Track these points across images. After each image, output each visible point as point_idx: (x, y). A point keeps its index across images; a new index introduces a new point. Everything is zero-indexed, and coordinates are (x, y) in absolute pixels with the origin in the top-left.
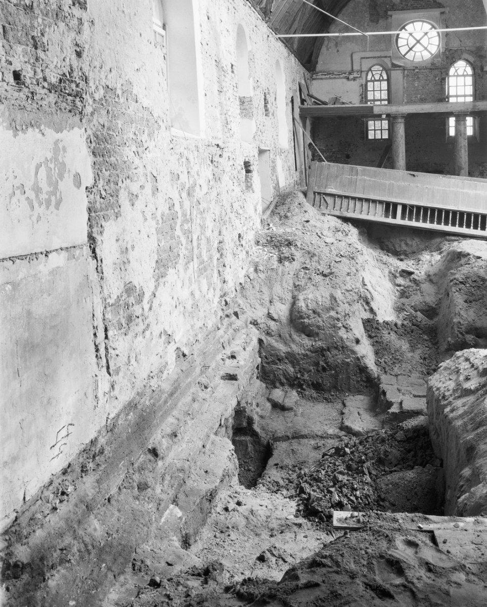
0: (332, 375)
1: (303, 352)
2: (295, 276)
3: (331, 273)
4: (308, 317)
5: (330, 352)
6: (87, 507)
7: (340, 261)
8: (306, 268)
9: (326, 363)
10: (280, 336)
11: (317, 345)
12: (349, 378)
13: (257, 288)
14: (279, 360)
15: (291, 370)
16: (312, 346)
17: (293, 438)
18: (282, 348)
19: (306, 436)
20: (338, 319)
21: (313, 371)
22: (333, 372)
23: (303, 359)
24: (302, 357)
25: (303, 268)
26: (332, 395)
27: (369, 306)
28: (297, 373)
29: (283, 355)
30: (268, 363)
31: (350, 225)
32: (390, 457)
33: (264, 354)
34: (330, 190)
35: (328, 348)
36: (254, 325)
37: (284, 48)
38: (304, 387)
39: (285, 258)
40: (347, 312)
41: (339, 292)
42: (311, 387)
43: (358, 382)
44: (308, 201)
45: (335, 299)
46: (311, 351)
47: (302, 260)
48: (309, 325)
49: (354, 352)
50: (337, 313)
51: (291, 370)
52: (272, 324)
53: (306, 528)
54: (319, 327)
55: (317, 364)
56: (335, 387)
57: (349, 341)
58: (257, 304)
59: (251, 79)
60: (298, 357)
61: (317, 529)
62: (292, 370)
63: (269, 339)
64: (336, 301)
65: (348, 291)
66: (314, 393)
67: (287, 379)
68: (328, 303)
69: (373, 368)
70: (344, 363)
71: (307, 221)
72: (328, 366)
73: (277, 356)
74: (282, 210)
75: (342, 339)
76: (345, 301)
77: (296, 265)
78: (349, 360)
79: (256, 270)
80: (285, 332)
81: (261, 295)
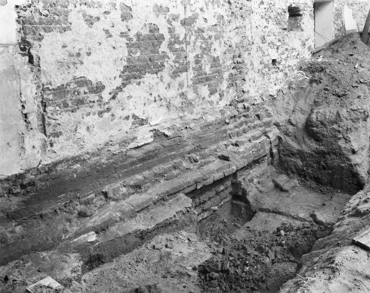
0: (329, 174)
1: (310, 152)
2: (317, 95)
3: (344, 95)
4: (317, 126)
5: (330, 156)
6: (7, 215)
7: (357, 87)
8: (327, 90)
9: (326, 164)
10: (296, 137)
11: (320, 149)
12: (342, 179)
13: (286, 100)
14: (292, 154)
15: (300, 163)
16: (317, 148)
17: (273, 212)
18: (295, 146)
19: (282, 213)
20: (339, 132)
21: (315, 167)
22: (330, 171)
23: (309, 157)
24: (309, 155)
25: (324, 89)
26: (327, 189)
28: (304, 166)
29: (296, 151)
30: (284, 155)
32: (299, 248)
33: (282, 148)
35: (328, 152)
36: (277, 126)
38: (307, 178)
39: (315, 80)
40: (349, 127)
41: (344, 110)
42: (313, 179)
43: (349, 183)
44: (362, 40)
45: (339, 115)
46: (315, 152)
47: (327, 83)
48: (317, 132)
49: (349, 160)
50: (339, 126)
51: (300, 163)
52: (290, 128)
53: (191, 280)
54: (323, 135)
55: (319, 163)
56: (331, 184)
57: (346, 150)
58: (282, 111)
60: (305, 154)
61: (198, 285)
62: (301, 163)
63: (287, 138)
64: (340, 117)
66: (314, 185)
67: (297, 169)
68: (333, 118)
69: (364, 175)
70: (339, 166)
71: (352, 55)
72: (327, 166)
73: (291, 151)
74: (335, 47)
75: (340, 147)
76: (349, 118)
77: (321, 86)
78: (344, 165)
79: (289, 88)
80: (300, 135)
81: (287, 106)
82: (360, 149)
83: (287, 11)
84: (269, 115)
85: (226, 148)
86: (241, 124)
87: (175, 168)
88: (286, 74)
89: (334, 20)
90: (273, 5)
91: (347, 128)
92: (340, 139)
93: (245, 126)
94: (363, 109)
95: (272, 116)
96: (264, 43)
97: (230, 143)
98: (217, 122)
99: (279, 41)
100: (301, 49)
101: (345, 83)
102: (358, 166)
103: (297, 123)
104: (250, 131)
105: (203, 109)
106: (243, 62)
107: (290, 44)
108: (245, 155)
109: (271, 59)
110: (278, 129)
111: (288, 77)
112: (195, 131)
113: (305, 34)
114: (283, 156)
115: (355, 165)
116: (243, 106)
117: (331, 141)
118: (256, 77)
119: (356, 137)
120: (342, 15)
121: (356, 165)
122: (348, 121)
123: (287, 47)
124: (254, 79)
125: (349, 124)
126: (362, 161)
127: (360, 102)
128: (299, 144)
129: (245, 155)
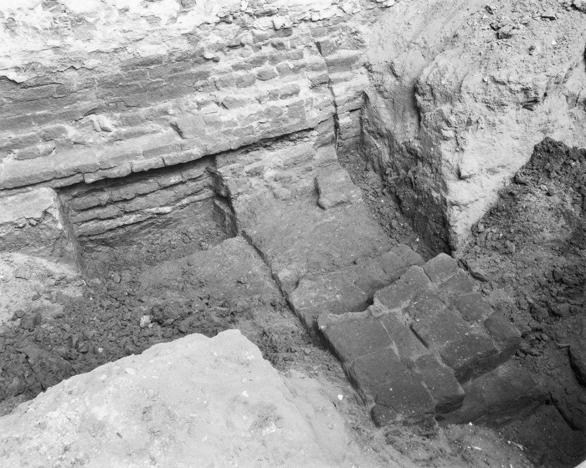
20: (448, 123)
29: (385, 132)
30: (369, 132)
33: (367, 117)
40: (474, 119)
43: (435, 234)
49: (446, 189)
52: (390, 79)
63: (380, 99)
76: (480, 97)
82: (484, 170)
84: (359, 44)
85: (199, 109)
86: (259, 62)
87: (46, 139)
92: (446, 139)
93: (267, 66)
94: (519, 84)
95: (364, 47)
97: (213, 98)
98: (174, 58)
102: (457, 208)
103: (403, 74)
104: (277, 78)
105: (124, 31)
108: (235, 128)
110: (370, 76)
112: (104, 75)
114: (367, 134)
115: (453, 204)
116: (271, 23)
117: (430, 137)
119: (483, 145)
121: (454, 205)
122: (477, 105)
125: (478, 110)
126: (473, 200)
127: (524, 65)
128: (395, 120)
129: (235, 128)
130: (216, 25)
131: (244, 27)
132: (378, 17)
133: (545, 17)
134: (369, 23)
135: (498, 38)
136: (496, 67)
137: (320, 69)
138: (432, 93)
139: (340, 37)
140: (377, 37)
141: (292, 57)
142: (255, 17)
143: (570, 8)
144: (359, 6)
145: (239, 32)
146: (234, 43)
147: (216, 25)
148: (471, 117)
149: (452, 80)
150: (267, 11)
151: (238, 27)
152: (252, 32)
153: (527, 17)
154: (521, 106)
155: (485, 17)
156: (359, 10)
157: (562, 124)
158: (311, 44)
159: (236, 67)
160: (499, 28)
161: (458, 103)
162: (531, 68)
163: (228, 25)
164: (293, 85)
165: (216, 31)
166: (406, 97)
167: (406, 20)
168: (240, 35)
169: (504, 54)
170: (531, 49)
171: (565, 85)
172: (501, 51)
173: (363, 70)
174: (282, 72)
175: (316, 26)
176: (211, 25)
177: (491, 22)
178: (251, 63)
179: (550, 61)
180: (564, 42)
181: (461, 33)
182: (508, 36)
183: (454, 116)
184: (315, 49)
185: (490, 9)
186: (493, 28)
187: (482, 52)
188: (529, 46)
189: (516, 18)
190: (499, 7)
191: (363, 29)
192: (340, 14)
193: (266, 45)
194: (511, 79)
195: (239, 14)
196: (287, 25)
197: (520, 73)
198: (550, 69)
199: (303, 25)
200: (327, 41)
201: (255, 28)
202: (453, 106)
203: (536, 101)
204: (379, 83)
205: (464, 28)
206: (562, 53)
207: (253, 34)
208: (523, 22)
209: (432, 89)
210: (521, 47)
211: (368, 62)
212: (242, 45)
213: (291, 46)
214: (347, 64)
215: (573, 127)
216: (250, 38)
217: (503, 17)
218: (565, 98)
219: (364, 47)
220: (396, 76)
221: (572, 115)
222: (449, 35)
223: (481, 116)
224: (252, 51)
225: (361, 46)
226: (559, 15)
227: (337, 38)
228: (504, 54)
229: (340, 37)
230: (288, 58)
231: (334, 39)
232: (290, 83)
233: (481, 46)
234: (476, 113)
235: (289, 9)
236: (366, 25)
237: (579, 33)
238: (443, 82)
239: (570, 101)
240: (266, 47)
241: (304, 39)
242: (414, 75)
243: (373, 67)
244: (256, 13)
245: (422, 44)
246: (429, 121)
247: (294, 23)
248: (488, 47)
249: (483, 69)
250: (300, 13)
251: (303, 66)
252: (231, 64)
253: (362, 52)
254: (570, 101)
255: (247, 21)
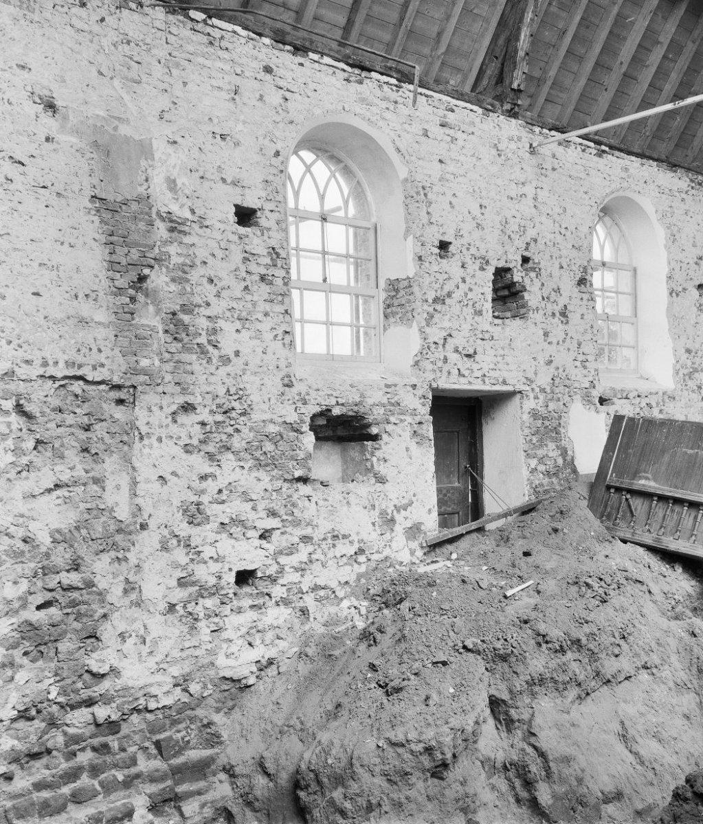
27: (529, 791)
31: (679, 570)
34: (642, 482)
37: (670, 174)
52: (261, 781)
59: (411, 238)
63: (249, 814)
65: (394, 744)
76: (377, 769)
83: (306, 428)
84: (214, 740)
86: (72, 775)
88: (304, 612)
89: (526, 447)
90: (244, 414)
91: (369, 801)
93: (85, 780)
95: (221, 743)
96: (199, 524)
99: (273, 514)
100: (374, 535)
101: (420, 648)
104: (101, 796)
106: (90, 584)
107: (321, 522)
109: (230, 570)
110: (232, 783)
111: (311, 619)
113: (393, 493)
118: (151, 627)
120: (562, 430)
123: (308, 531)
124: (142, 632)
127: (421, 718)
130: (12, 723)
131: (52, 723)
132: (237, 701)
133: (437, 663)
134: (226, 710)
135: (388, 696)
136: (390, 726)
137: (162, 779)
138: (318, 781)
139: (187, 732)
140: (238, 727)
141: (121, 765)
142: (68, 709)
143: (461, 650)
144: (210, 686)
145: (45, 732)
146: (36, 750)
147: (12, 723)
148: (371, 798)
149: (341, 755)
150: (85, 698)
151: (43, 725)
152: (63, 731)
153: (417, 665)
154: (429, 775)
155: (369, 675)
156: (211, 691)
157: (485, 800)
158: (147, 744)
159: (39, 786)
160: (387, 685)
161: (351, 783)
162: (430, 720)
163: (29, 723)
164: (124, 804)
165: (11, 732)
166: (286, 803)
167: (274, 699)
168: (46, 737)
169: (396, 709)
170: (427, 698)
171: (476, 746)
172: (394, 707)
173: (223, 776)
174: (108, 788)
175: (154, 718)
176: (4, 723)
177: (377, 680)
178: (61, 777)
179: (449, 709)
180: (462, 688)
181: (345, 701)
182: (398, 690)
183: (349, 801)
184: (154, 751)
185: (374, 666)
186: (380, 686)
187: (371, 713)
188: (424, 697)
189: (404, 670)
190: (384, 662)
191: (218, 718)
192: (185, 698)
193: (83, 750)
194: (410, 737)
195: (45, 705)
196: (114, 717)
197: (419, 729)
198: (451, 719)
199: (135, 718)
200: (171, 738)
201: (67, 725)
202: (346, 788)
203: (445, 765)
204: (247, 789)
205: (346, 694)
206: (462, 699)
207: (65, 734)
208: (413, 672)
209: (316, 775)
210: (415, 699)
211: (229, 763)
212: (49, 752)
213: (119, 748)
214: (200, 769)
215: (497, 803)
216: (60, 739)
217: (390, 671)
218: (479, 763)
219: (221, 743)
220: (268, 775)
221: (493, 788)
222: (330, 707)
223: (382, 795)
224: (63, 761)
225: (218, 743)
226: (452, 659)
227: (184, 733)
228: (396, 709)
229: (187, 732)
230: (116, 766)
231: (179, 735)
232: (118, 804)
233: (369, 707)
234: (376, 793)
235: (116, 694)
236: (222, 713)
237: (477, 678)
238: (330, 761)
239: (487, 769)
240: (82, 753)
241: (137, 738)
242: (292, 769)
243: (236, 768)
244: (70, 703)
245: (299, 726)
246: (319, 819)
247: (123, 714)
248: (377, 706)
249: (375, 733)
250: (131, 699)
251: (137, 776)
252: (32, 781)
253: (219, 751)
254: (487, 769)
255: (56, 714)
